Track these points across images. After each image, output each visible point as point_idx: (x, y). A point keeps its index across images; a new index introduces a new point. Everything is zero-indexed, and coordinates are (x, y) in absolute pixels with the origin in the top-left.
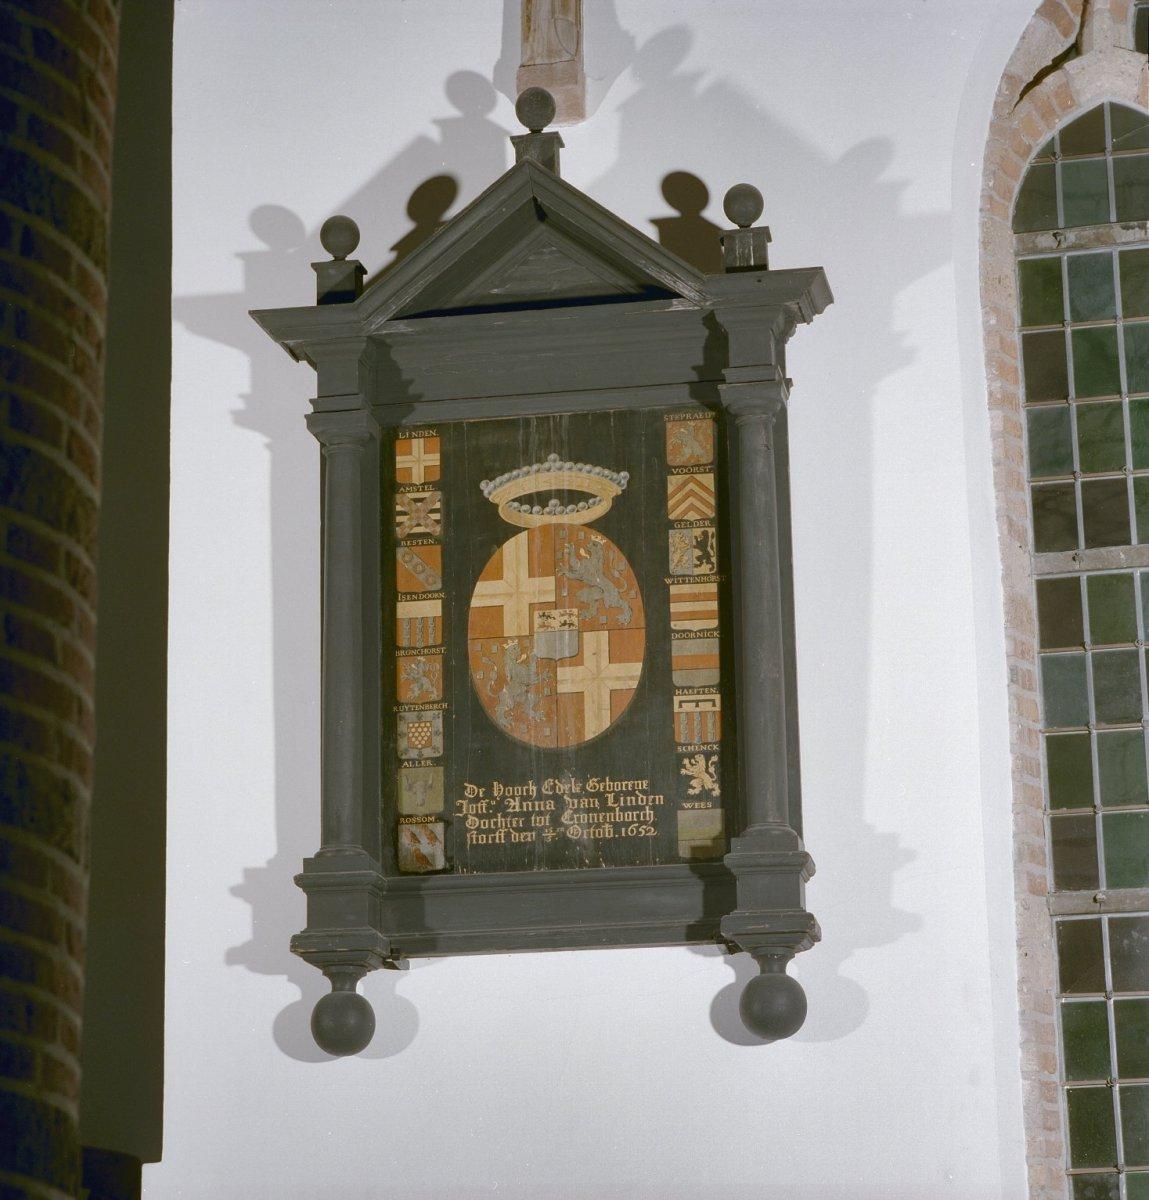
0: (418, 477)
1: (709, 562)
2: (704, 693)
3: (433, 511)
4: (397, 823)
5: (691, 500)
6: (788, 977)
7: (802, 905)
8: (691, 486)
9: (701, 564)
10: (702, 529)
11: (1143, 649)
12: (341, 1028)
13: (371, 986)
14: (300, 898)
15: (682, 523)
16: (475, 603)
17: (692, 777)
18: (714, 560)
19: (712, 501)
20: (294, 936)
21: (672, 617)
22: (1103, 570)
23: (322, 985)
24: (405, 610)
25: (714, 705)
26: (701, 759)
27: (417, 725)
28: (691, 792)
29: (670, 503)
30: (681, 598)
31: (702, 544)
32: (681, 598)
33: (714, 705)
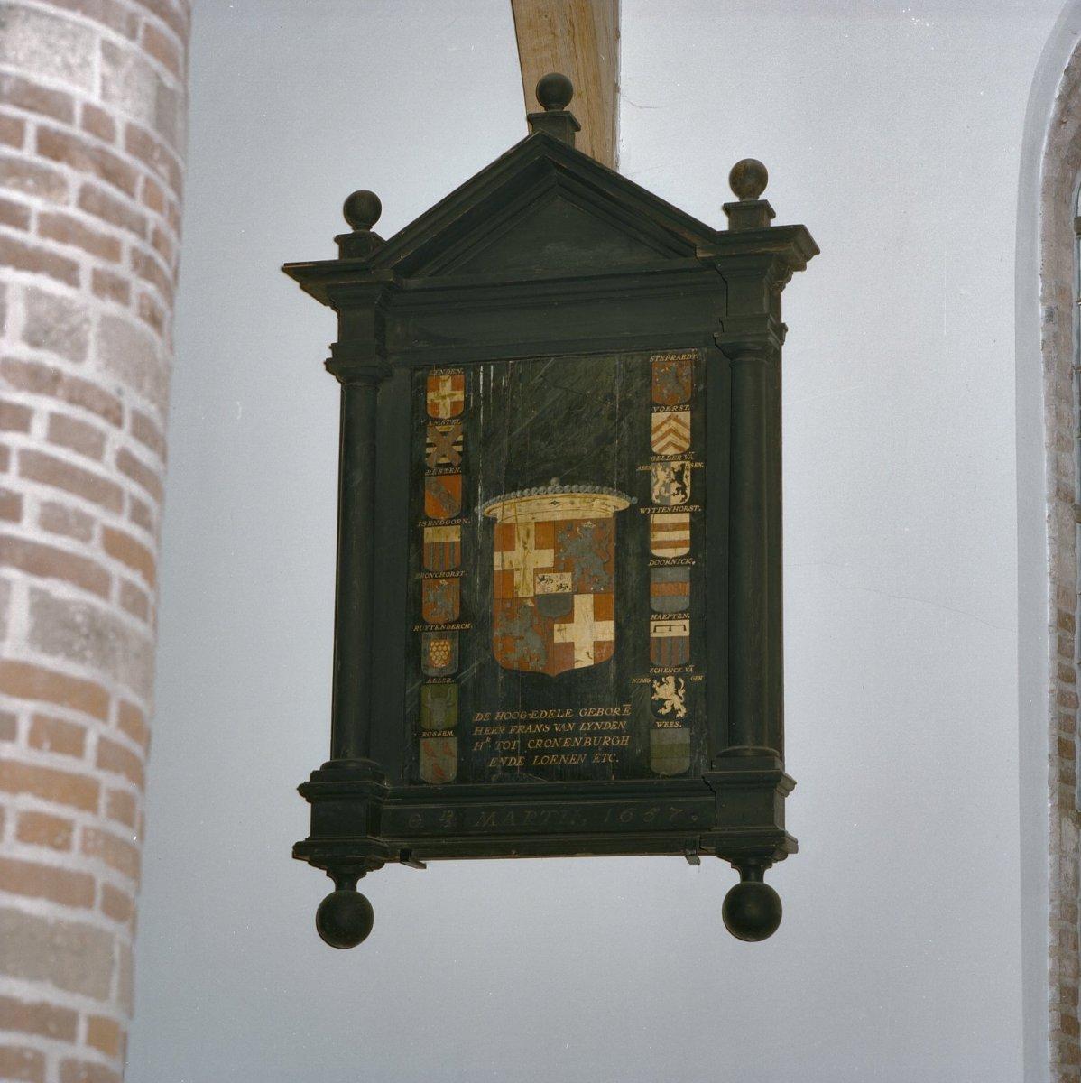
0: (444, 413)
1: (684, 493)
2: (676, 619)
3: (457, 444)
4: (419, 736)
5: (670, 438)
6: (360, 895)
7: (777, 820)
8: (673, 424)
9: (678, 494)
10: (681, 462)
11: (35, 76)
12: (344, 922)
13: (365, 886)
14: (304, 809)
15: (666, 460)
16: (688, 549)
17: (664, 700)
18: (688, 491)
19: (687, 434)
20: (297, 843)
21: (689, 544)
22: (1076, 572)
23: (321, 885)
24: (431, 535)
25: (685, 629)
26: (671, 679)
27: (437, 644)
28: (663, 711)
29: (654, 438)
30: (662, 528)
31: (679, 476)
32: (662, 528)
33: (685, 629)
